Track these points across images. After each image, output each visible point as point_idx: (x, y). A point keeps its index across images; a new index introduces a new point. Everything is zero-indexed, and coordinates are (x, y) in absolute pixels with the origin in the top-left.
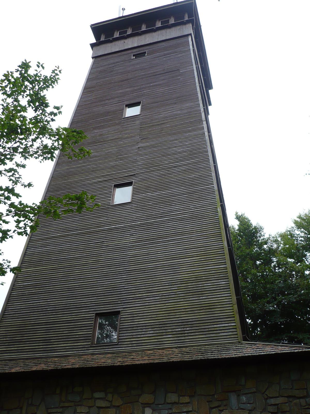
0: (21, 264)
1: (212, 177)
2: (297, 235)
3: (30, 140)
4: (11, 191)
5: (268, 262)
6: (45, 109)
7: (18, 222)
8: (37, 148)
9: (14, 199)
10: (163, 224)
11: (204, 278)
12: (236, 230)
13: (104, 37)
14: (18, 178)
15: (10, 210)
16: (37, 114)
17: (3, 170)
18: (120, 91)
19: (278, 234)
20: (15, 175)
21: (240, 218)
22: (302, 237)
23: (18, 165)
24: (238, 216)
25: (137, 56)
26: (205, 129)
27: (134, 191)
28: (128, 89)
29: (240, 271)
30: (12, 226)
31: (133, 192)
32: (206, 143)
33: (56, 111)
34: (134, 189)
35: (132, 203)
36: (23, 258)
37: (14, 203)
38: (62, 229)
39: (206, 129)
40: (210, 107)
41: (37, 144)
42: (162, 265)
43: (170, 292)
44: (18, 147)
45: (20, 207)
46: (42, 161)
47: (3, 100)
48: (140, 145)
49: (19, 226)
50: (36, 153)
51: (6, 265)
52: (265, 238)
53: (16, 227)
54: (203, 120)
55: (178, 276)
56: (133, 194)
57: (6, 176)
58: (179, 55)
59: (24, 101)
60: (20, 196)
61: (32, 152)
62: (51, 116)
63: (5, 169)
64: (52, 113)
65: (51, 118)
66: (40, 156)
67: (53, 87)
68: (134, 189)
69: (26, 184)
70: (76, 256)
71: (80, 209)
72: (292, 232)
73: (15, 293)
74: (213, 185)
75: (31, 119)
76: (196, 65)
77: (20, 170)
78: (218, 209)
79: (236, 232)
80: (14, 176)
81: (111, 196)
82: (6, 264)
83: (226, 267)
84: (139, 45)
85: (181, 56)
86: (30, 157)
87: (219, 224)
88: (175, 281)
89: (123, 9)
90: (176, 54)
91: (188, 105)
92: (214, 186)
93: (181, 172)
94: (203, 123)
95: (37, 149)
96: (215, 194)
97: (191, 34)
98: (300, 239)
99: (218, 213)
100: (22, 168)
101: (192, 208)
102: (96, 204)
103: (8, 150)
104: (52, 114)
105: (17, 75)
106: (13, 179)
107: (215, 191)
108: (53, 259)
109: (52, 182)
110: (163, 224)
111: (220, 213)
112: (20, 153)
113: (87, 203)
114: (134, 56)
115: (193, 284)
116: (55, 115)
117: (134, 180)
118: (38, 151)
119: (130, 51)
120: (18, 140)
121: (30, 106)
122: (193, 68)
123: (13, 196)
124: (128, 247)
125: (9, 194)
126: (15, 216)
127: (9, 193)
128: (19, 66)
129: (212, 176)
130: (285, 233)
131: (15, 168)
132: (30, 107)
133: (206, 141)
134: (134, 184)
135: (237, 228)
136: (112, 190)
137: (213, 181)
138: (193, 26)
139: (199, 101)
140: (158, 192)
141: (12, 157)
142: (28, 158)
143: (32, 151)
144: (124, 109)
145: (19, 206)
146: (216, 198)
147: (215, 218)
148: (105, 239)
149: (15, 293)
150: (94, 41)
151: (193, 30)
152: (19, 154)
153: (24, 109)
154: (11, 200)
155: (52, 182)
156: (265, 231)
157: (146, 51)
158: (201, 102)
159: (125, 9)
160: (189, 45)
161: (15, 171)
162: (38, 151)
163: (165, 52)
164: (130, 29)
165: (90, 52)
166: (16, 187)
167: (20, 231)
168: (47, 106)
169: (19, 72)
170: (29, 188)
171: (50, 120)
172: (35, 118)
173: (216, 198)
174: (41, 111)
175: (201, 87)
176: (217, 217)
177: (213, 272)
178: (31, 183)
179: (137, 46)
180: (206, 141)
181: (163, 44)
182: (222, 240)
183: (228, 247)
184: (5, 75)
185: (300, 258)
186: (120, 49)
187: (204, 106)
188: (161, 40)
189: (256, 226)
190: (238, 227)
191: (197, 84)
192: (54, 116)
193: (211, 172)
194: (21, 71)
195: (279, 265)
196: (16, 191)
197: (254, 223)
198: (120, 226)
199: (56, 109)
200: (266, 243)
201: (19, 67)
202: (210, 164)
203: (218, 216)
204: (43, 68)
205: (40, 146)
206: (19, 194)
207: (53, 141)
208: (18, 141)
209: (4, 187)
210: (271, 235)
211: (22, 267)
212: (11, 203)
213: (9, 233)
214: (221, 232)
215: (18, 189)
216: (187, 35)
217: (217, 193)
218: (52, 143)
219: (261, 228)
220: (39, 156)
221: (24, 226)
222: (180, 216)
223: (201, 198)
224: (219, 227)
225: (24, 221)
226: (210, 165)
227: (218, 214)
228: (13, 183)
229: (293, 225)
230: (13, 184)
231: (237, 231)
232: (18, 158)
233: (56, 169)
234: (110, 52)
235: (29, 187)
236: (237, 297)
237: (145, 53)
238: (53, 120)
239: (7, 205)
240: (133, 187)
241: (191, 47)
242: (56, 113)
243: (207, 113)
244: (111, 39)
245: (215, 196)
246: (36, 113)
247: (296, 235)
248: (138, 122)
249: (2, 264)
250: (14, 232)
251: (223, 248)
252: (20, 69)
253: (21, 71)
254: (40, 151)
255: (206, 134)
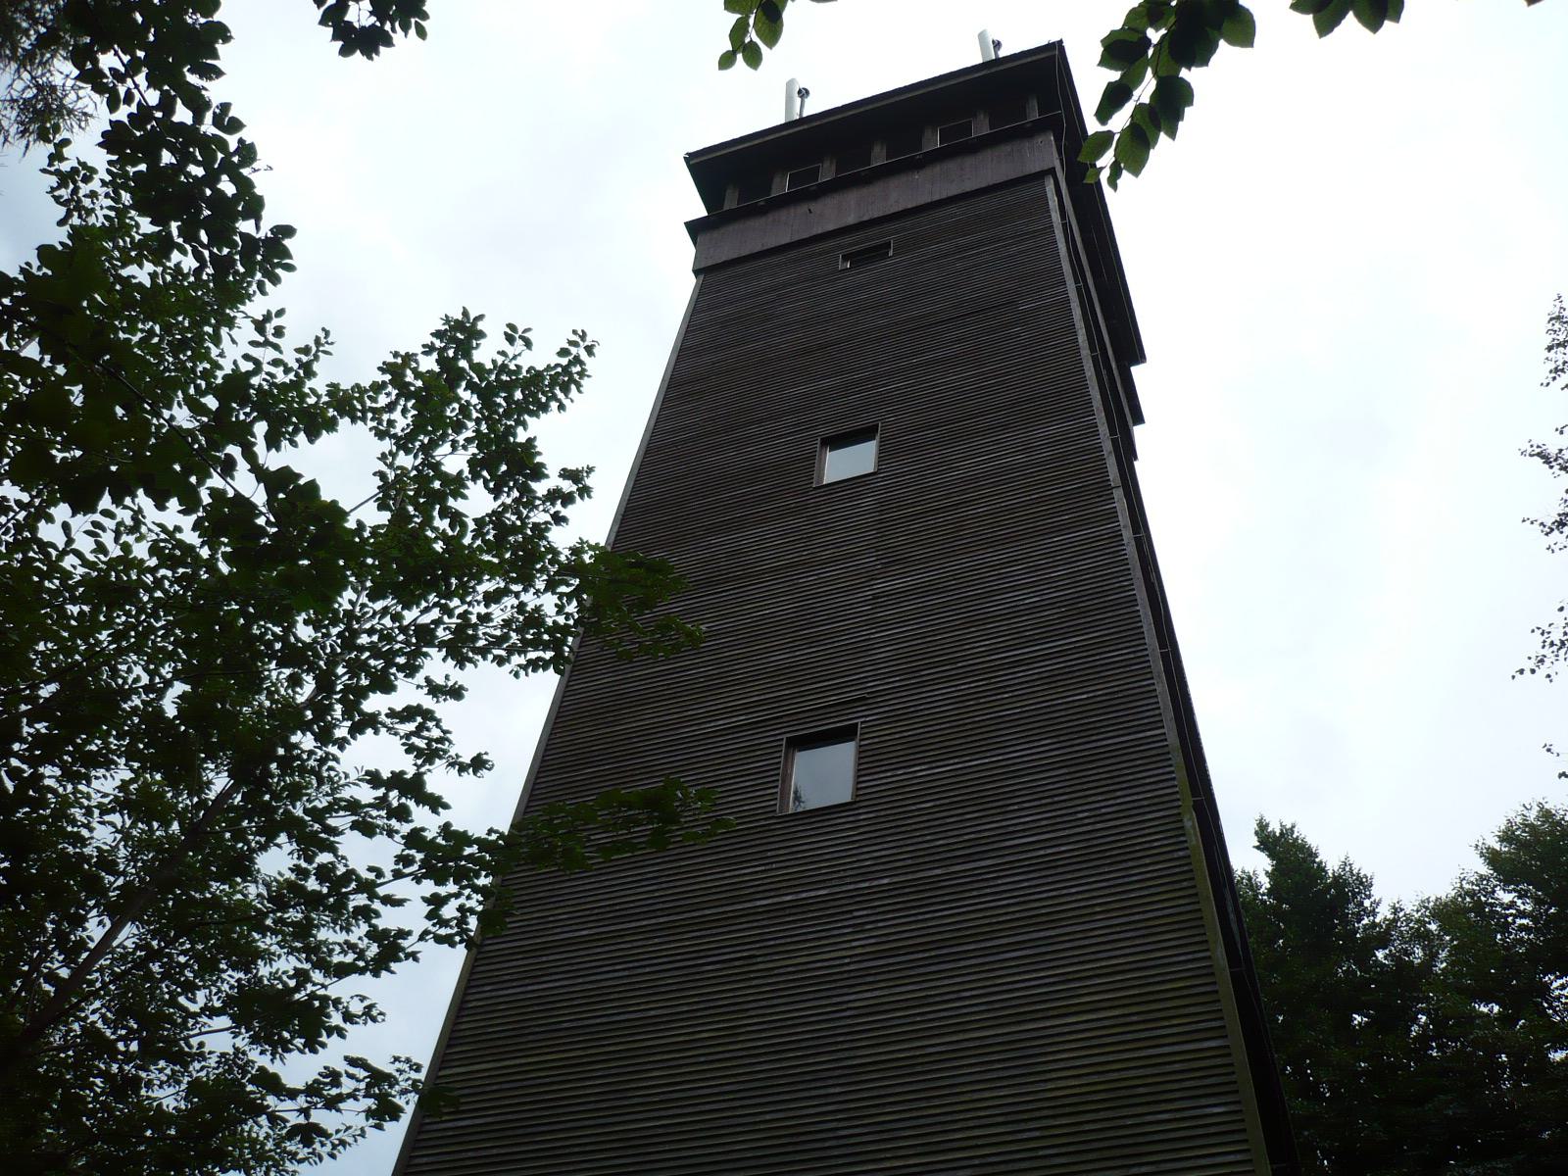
0: (449, 1046)
1: (1155, 700)
2: (1505, 909)
3: (480, 598)
4: (413, 787)
5: (1392, 1018)
6: (529, 486)
7: (436, 902)
8: (502, 623)
9: (422, 817)
10: (976, 886)
11: (1142, 1090)
12: (1263, 895)
13: (737, 194)
14: (440, 740)
15: (408, 855)
16: (503, 504)
17: (383, 713)
18: (802, 389)
19: (1427, 908)
20: (428, 730)
21: (1272, 842)
22: (1522, 914)
23: (434, 690)
24: (1268, 836)
25: (858, 258)
26: (1120, 518)
27: (862, 761)
28: (826, 383)
29: (1284, 1057)
30: (410, 917)
31: (860, 752)
32: (1129, 569)
33: (568, 486)
34: (863, 769)
35: (855, 806)
36: (456, 1024)
37: (423, 829)
38: (596, 911)
39: (1124, 518)
40: (1138, 431)
41: (499, 613)
42: (977, 1043)
43: (1014, 1147)
44: (438, 622)
45: (444, 843)
46: (522, 673)
47: (383, 457)
48: (880, 586)
49: (439, 917)
50: (499, 641)
51: (407, 1080)
52: (1377, 920)
53: (429, 917)
54: (1113, 485)
55: (1043, 1086)
56: (859, 770)
57: (396, 734)
58: (1014, 249)
59: (454, 462)
60: (446, 806)
61: (486, 640)
62: (553, 504)
63: (389, 709)
64: (554, 495)
65: (552, 512)
66: (513, 654)
67: (562, 407)
68: (863, 769)
69: (466, 759)
70: (653, 1013)
71: (659, 840)
72: (1485, 896)
73: (425, 1160)
74: (1163, 727)
75: (480, 522)
76: (1076, 281)
77: (444, 709)
78: (1185, 820)
79: (1263, 902)
80: (425, 734)
81: (778, 780)
82: (406, 1076)
83: (1228, 1047)
84: (865, 218)
85: (1020, 252)
86: (479, 657)
87: (1193, 879)
88: (1030, 1107)
89: (804, 93)
90: (1002, 247)
91: (1053, 429)
92: (1165, 734)
93: (1038, 683)
94: (1114, 495)
95: (503, 627)
96: (1170, 762)
97: (1052, 172)
98: (1519, 921)
99: (1183, 835)
100: (451, 702)
101: (1087, 821)
102: (718, 820)
103: (401, 637)
104: (558, 498)
105: (429, 364)
106: (421, 743)
107: (1168, 753)
108: (565, 1025)
109: (558, 735)
110: (976, 886)
111: (1193, 838)
112: (442, 645)
113: (686, 816)
114: (845, 258)
115: (1102, 1115)
116: (568, 499)
117: (863, 720)
118: (507, 633)
119: (831, 243)
120: (437, 599)
121: (475, 476)
122: (1065, 292)
123: (418, 804)
124: (846, 976)
125: (403, 800)
126: (425, 876)
127: (402, 794)
128: (437, 334)
129: (1156, 696)
130: (1454, 900)
131: (428, 702)
132: (478, 482)
133: (1126, 562)
134: (861, 734)
135: (1265, 883)
136: (782, 759)
137: (1160, 714)
138: (1058, 140)
139: (1094, 415)
140: (952, 761)
141: (415, 660)
142: (470, 660)
143: (484, 634)
144: (817, 453)
145: (440, 840)
146: (1174, 779)
147: (1176, 855)
148: (758, 945)
149: (425, 1160)
150: (699, 211)
151: (1060, 154)
152: (437, 649)
153: (455, 485)
154: (412, 821)
155: (558, 735)
156: (1376, 892)
157: (892, 239)
158: (1100, 418)
159: (807, 92)
160: (1048, 211)
161: (428, 715)
162: (507, 633)
163: (961, 241)
164: (829, 162)
165: (686, 251)
166: (429, 770)
167: (443, 931)
168: (538, 473)
169: (435, 356)
170: (479, 774)
171: (549, 519)
172: (496, 517)
173: (1174, 779)
174: (516, 494)
175: (1100, 362)
176: (1181, 854)
177: (1177, 1067)
178: (485, 757)
179: (855, 225)
180: (1128, 564)
181: (952, 210)
182: (1206, 941)
183: (1230, 968)
184: (386, 368)
185: (1527, 997)
186: (796, 238)
187: (1112, 431)
188: (944, 196)
189: (1340, 876)
190: (1268, 880)
191: (1085, 352)
192: (564, 505)
193: (1152, 678)
194: (442, 351)
195: (1440, 1030)
196: (430, 788)
197: (1331, 860)
198: (813, 894)
199: (569, 479)
200: (1383, 940)
201: (437, 338)
202: (1146, 649)
203: (1187, 848)
204: (528, 344)
205: (516, 615)
206: (439, 798)
207: (561, 596)
208: (436, 605)
209: (386, 775)
210: (1402, 910)
211: (450, 1058)
212: (412, 830)
213: (404, 943)
214: (1200, 910)
215: (438, 779)
216: (1040, 176)
217: (1177, 759)
218: (556, 605)
219: (1362, 883)
220: (511, 651)
221: (459, 915)
222: (1042, 852)
223: (1117, 780)
224: (1191, 892)
225: (457, 896)
226: (1145, 653)
227: (1186, 841)
228: (417, 757)
229: (1485, 870)
230: (419, 762)
231: (1265, 897)
232: (437, 666)
233: (571, 683)
234: (758, 248)
235: (475, 773)
236: (1275, 1166)
237: (888, 245)
238: (559, 519)
239: (397, 837)
240: (860, 746)
241: (1056, 217)
242: (571, 494)
243: (1126, 452)
244: (761, 201)
245: (1172, 772)
246: (499, 502)
247: (1499, 909)
248: (868, 502)
249: (389, 1076)
250: (422, 938)
251: (1213, 974)
252: (438, 343)
253: (442, 351)
254: (513, 635)
255: (1127, 535)
